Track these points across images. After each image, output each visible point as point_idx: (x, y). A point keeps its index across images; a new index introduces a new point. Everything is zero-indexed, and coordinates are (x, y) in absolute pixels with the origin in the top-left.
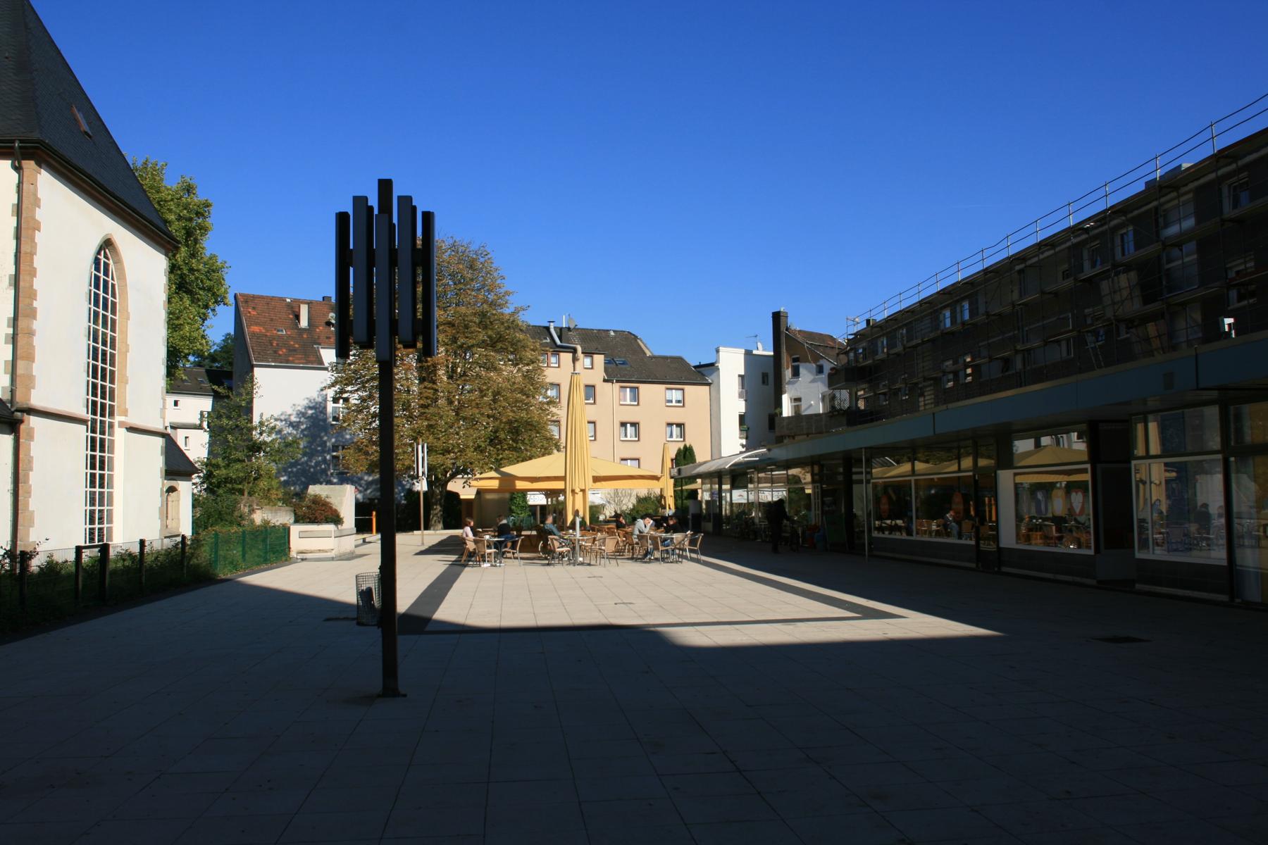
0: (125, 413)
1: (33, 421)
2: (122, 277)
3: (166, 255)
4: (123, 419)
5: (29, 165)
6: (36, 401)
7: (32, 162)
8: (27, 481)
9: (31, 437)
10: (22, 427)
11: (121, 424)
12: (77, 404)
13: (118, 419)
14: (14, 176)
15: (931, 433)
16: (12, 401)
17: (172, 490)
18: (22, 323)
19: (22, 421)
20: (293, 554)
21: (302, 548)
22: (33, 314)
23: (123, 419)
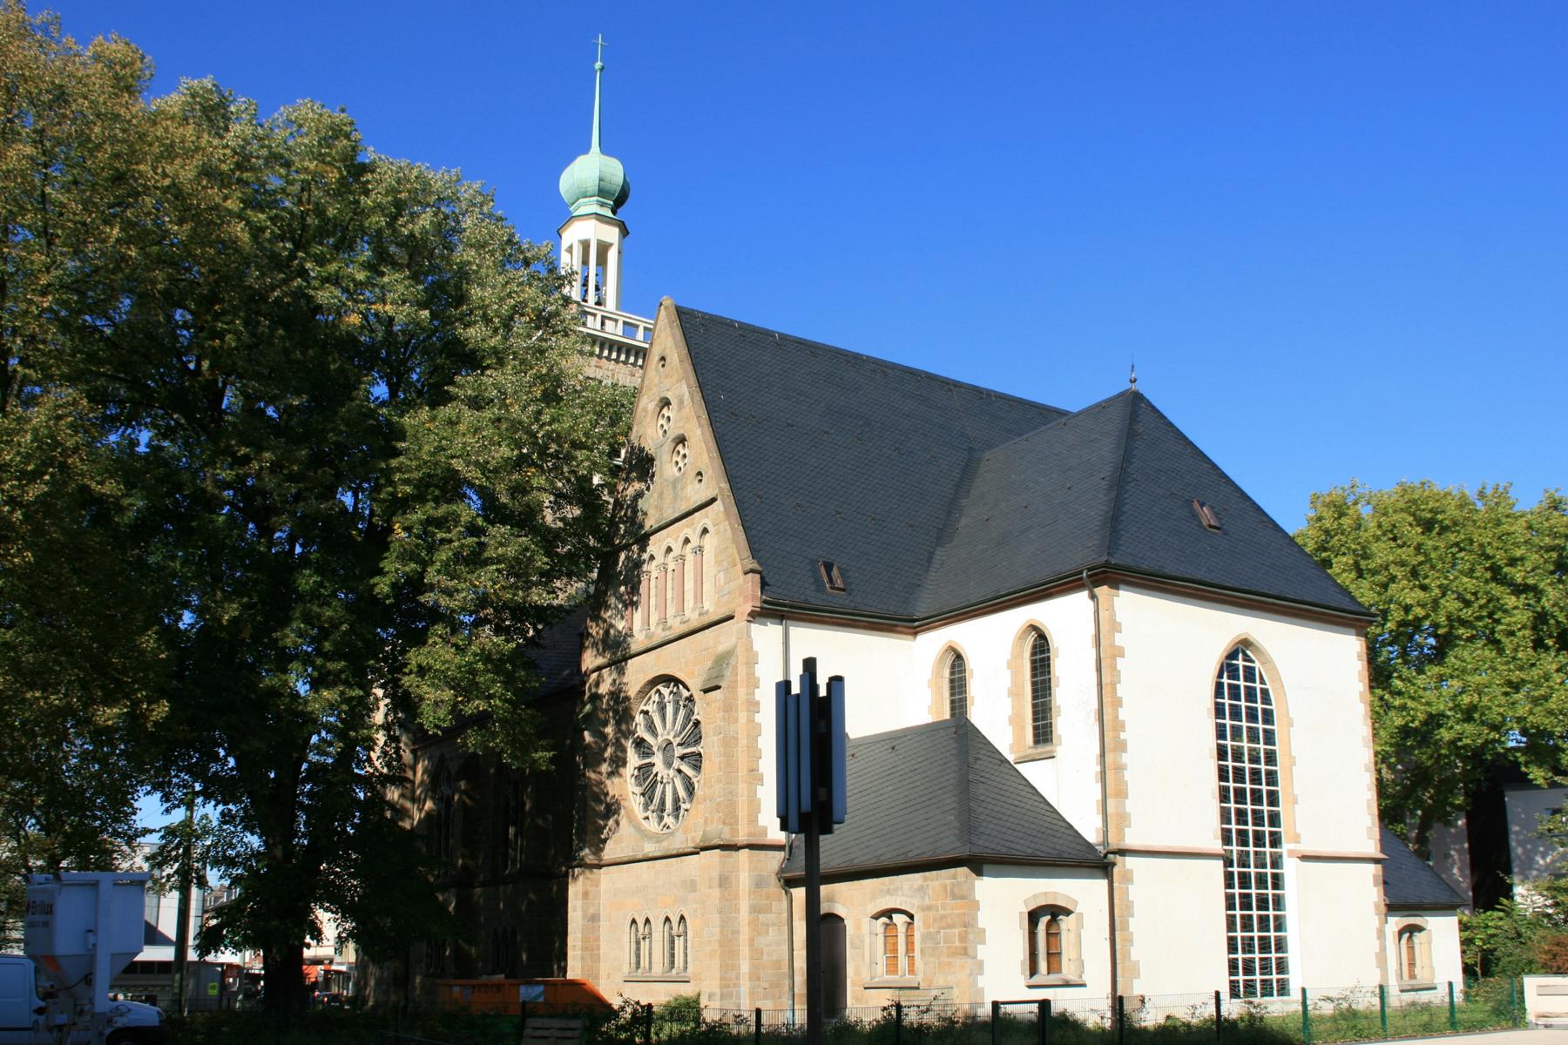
0: (1297, 839)
1: (1130, 861)
2: (1277, 678)
3: (1358, 635)
4: (1292, 846)
5: (1103, 591)
6: (1131, 840)
7: (1105, 588)
8: (1125, 927)
9: (1128, 878)
10: (1116, 870)
11: (1291, 853)
12: (172, 935)
13: (1285, 848)
14: (1091, 604)
15: (1372, 870)
16: (1105, 842)
17: (1412, 930)
18: (1109, 758)
19: (1114, 864)
20: (1530, 1017)
21: (1543, 1010)
22: (1122, 747)
23: (1292, 846)
